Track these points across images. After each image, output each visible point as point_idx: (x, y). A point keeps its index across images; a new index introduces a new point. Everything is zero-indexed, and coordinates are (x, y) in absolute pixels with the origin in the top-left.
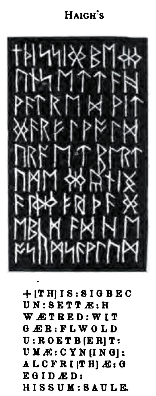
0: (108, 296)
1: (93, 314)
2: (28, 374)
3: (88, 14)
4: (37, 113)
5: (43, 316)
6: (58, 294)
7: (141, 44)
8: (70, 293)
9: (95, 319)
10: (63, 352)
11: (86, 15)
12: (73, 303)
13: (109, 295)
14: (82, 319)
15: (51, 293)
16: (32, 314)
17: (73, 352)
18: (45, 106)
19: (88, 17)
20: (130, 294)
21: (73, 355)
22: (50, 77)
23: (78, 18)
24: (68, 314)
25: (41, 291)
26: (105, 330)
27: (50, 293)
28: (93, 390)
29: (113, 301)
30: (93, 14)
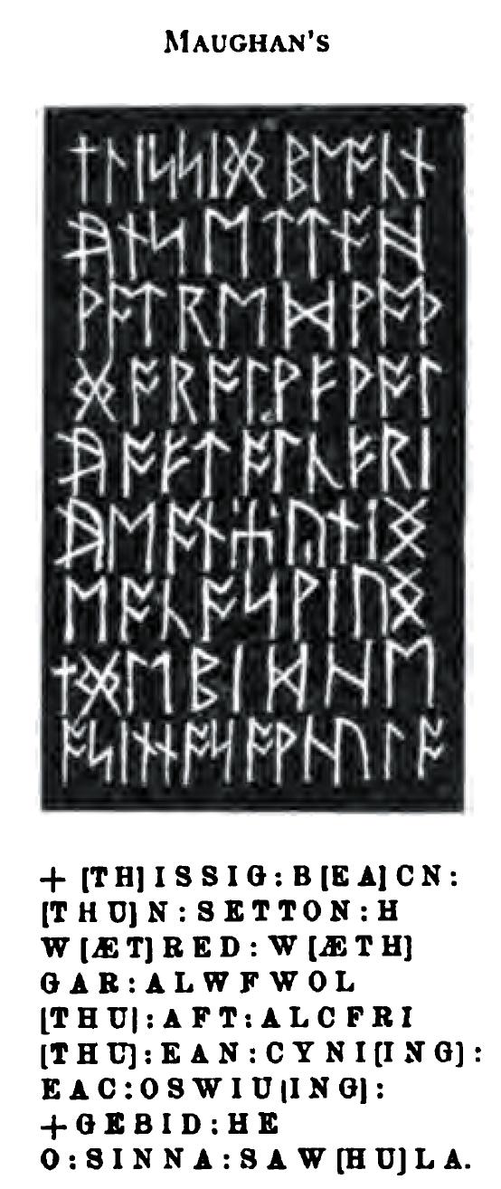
0: (297, 883)
1: (273, 938)
2: (275, 1118)
3: (243, 37)
4: (256, 336)
5: (111, 946)
6: (150, 877)
7: (443, 126)
8: (210, 875)
9: (50, 954)
10: (276, 1053)
11: (238, 42)
12: (274, 904)
13: (303, 880)
14: (235, 953)
15: (125, 876)
16: (68, 939)
17: (304, 1053)
18: (166, 311)
19: (243, 46)
20: (410, 876)
21: (304, 1060)
22: (179, 234)
23: (282, 49)
24: (195, 938)
25: (101, 871)
26: (185, 987)
27: (125, 876)
28: (271, 1167)
29: (411, 900)
30: (258, 39)
